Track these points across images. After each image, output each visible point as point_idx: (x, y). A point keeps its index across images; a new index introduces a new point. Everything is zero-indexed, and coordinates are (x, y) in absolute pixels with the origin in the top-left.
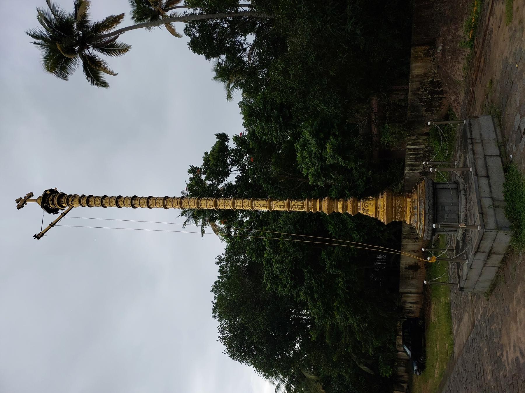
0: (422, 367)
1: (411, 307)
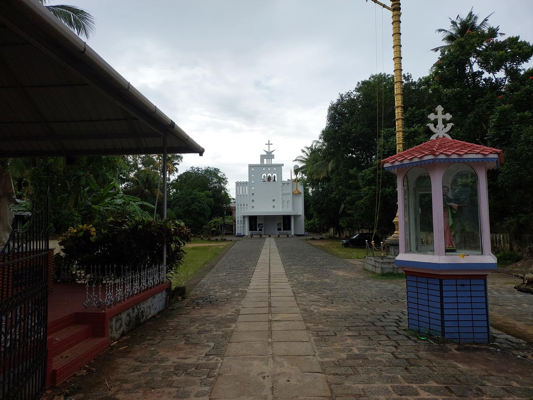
0: (346, 245)
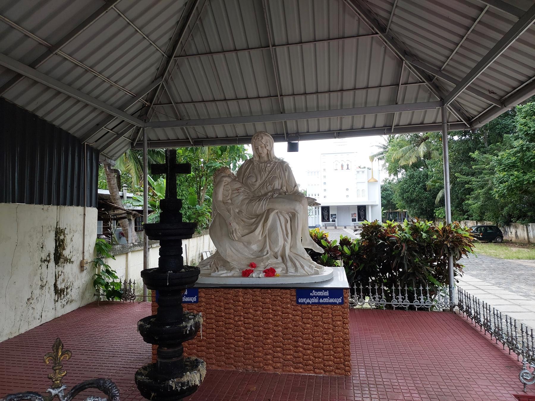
1: (511, 233)
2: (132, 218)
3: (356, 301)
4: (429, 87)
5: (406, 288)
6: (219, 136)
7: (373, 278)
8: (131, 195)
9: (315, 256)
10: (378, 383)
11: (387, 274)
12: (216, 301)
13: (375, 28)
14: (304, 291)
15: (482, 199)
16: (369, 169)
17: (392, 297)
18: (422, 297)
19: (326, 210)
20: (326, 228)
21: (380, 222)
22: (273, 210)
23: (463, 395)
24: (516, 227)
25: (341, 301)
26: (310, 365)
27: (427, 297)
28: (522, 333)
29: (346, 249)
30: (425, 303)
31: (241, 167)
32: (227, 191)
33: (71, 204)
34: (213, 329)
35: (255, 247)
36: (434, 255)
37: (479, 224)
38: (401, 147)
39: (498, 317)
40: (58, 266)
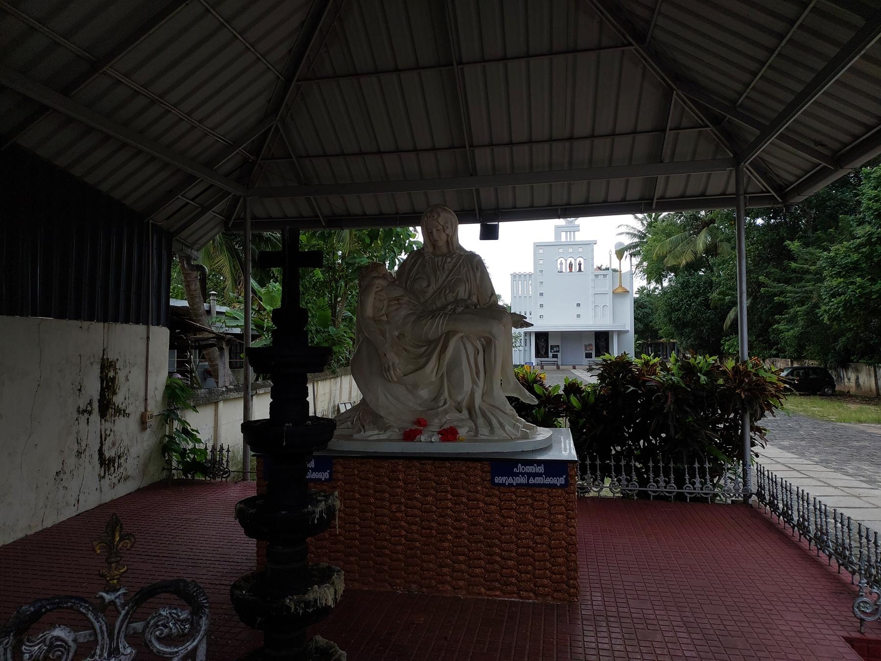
1: (849, 379)
2: (224, 346)
3: (589, 484)
4: (716, 135)
5: (672, 465)
6: (367, 213)
7: (619, 448)
8: (224, 309)
9: (523, 409)
10: (621, 615)
11: (642, 442)
12: (361, 479)
13: (628, 37)
14: (504, 465)
15: (801, 323)
16: (615, 271)
17: (648, 478)
18: (698, 480)
19: (542, 338)
20: (542, 368)
21: (631, 356)
22: (455, 333)
23: (761, 636)
24: (857, 370)
25: (563, 482)
26: (512, 583)
27: (706, 480)
28: (860, 539)
29: (574, 400)
30: (702, 489)
31: (403, 265)
32: (380, 301)
33: (127, 321)
34: (355, 523)
35: (424, 393)
36: (719, 412)
37: (795, 365)
38: (669, 235)
39: (821, 512)
40: (105, 421)
